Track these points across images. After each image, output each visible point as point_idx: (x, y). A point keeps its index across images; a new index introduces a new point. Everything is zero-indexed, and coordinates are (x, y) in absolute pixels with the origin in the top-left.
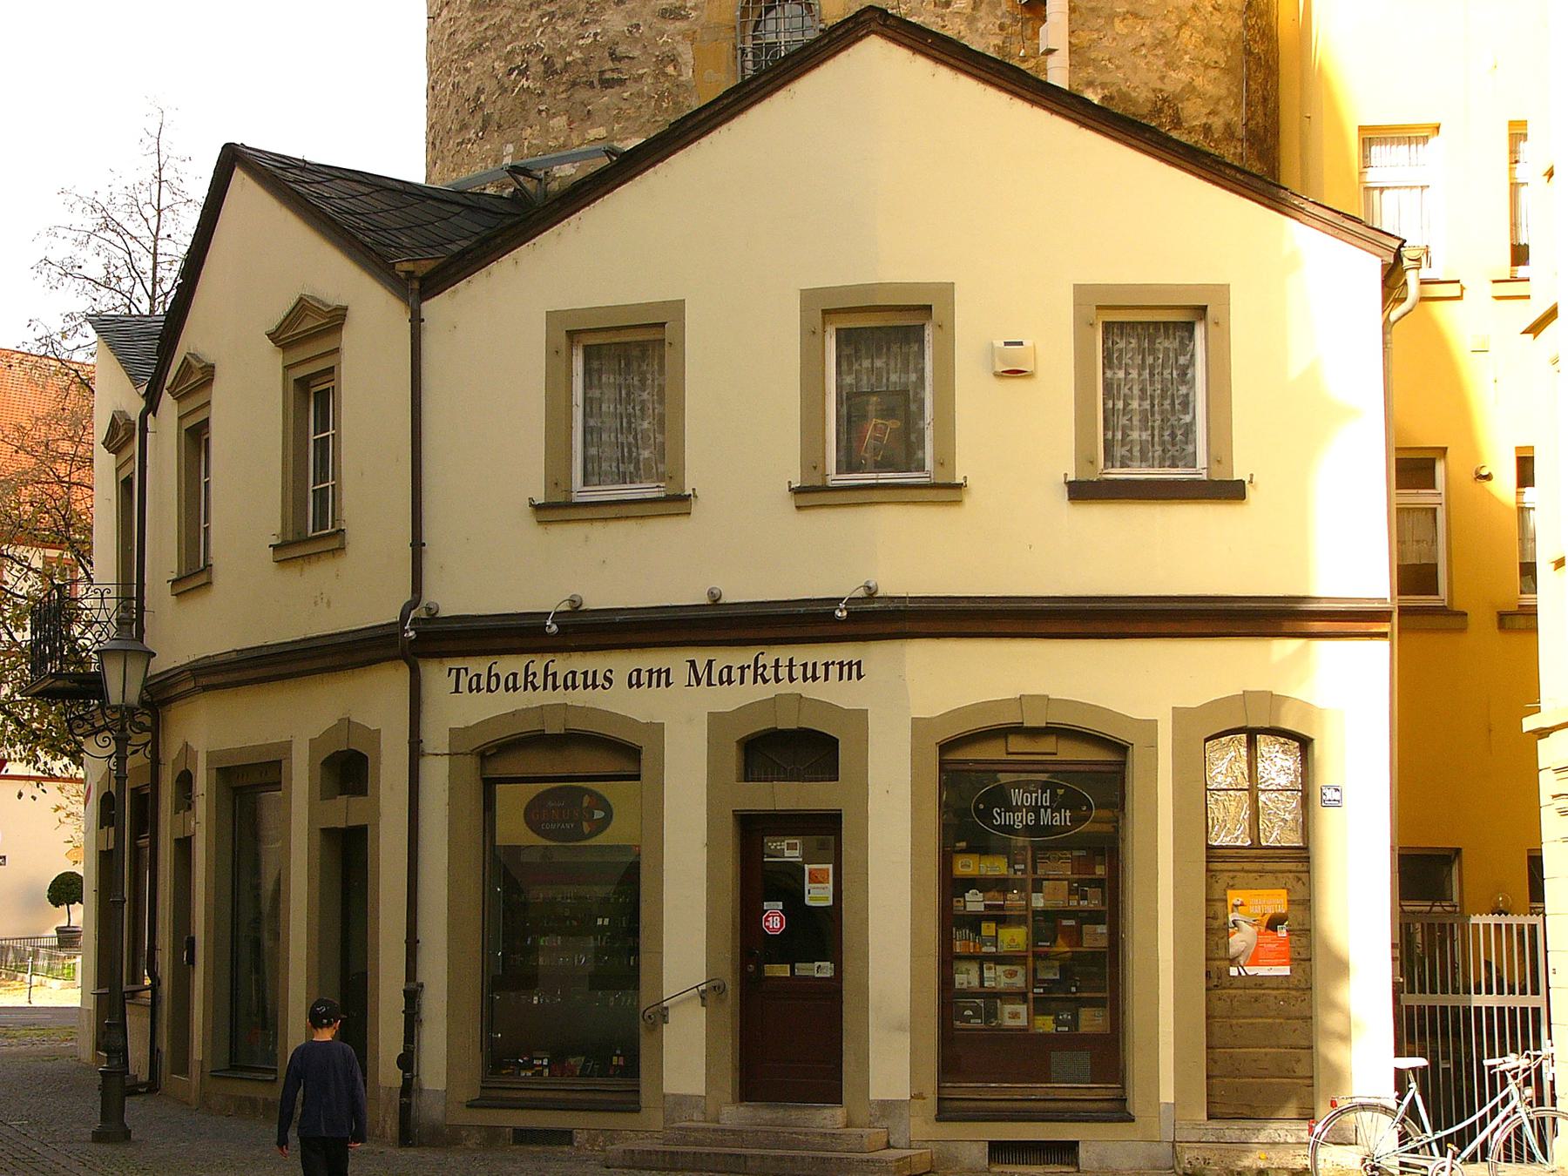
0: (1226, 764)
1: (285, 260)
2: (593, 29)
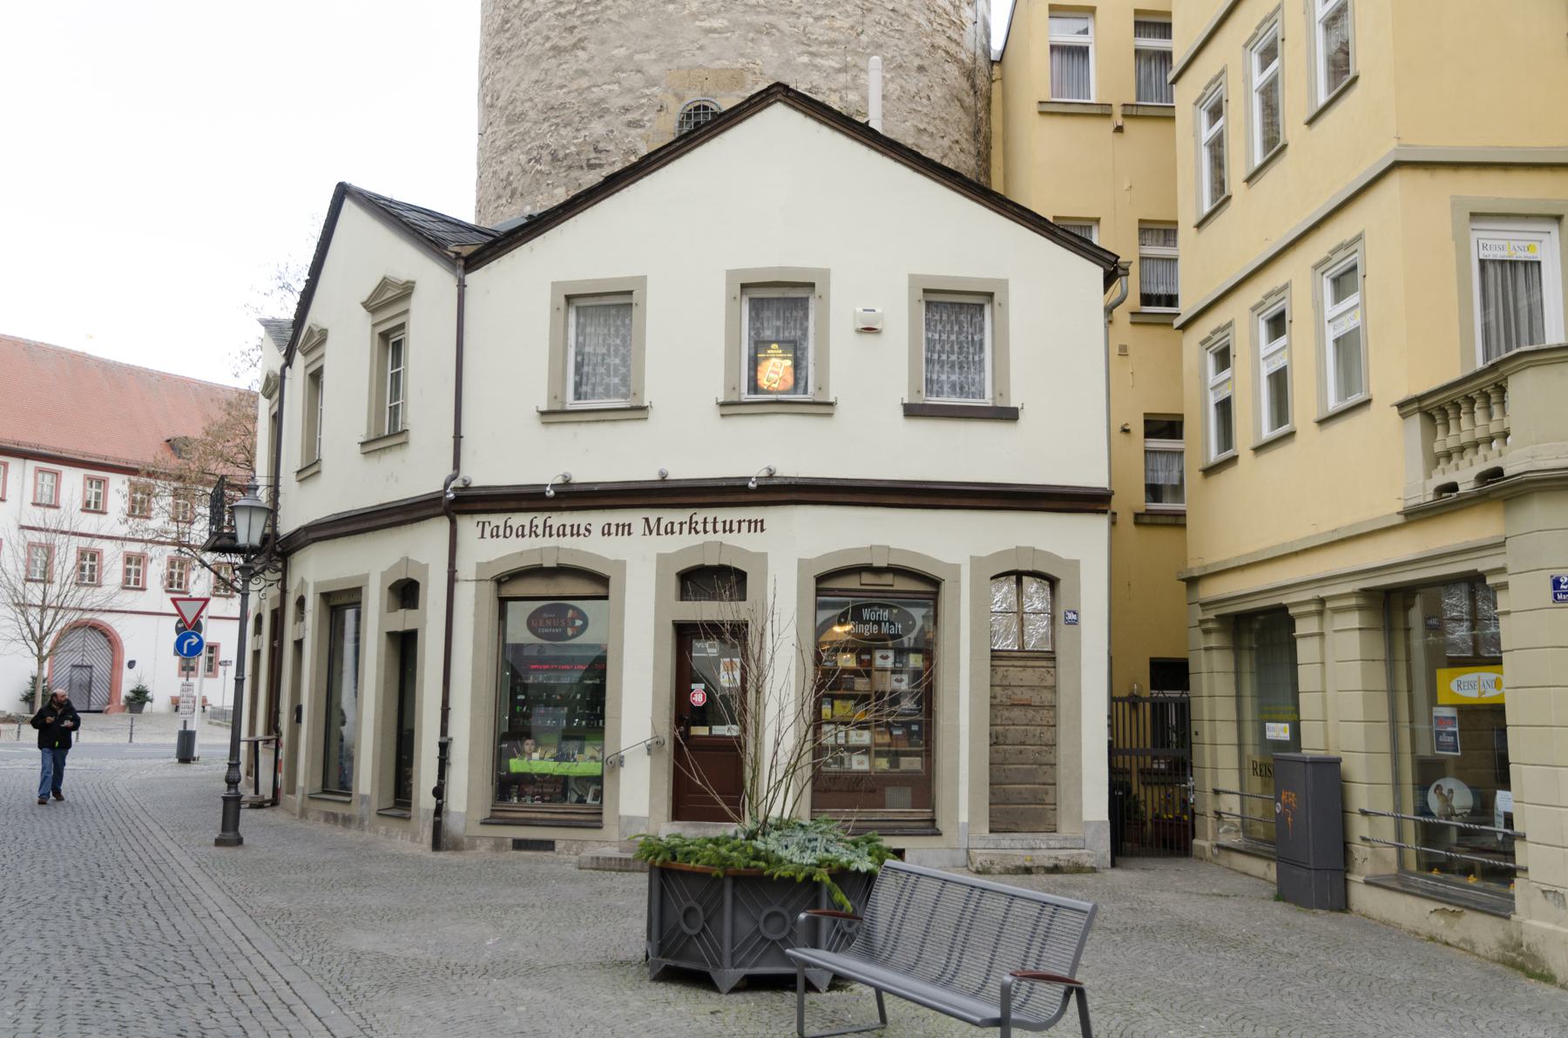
0: (1003, 594)
1: (372, 253)
2: (583, 133)
